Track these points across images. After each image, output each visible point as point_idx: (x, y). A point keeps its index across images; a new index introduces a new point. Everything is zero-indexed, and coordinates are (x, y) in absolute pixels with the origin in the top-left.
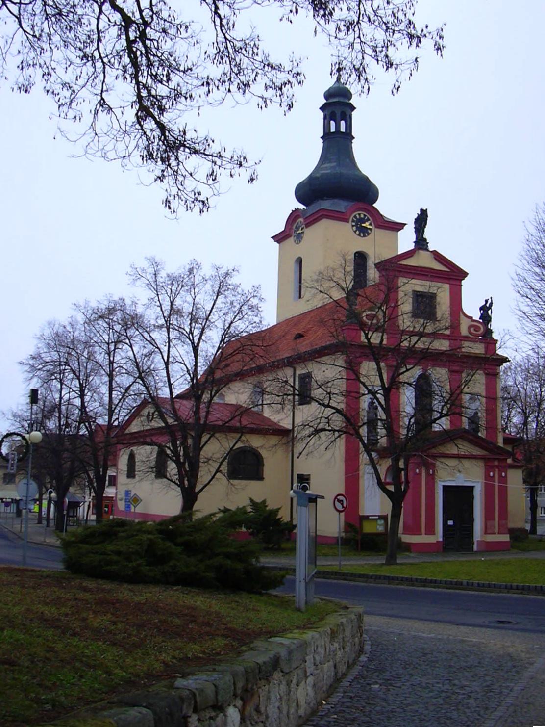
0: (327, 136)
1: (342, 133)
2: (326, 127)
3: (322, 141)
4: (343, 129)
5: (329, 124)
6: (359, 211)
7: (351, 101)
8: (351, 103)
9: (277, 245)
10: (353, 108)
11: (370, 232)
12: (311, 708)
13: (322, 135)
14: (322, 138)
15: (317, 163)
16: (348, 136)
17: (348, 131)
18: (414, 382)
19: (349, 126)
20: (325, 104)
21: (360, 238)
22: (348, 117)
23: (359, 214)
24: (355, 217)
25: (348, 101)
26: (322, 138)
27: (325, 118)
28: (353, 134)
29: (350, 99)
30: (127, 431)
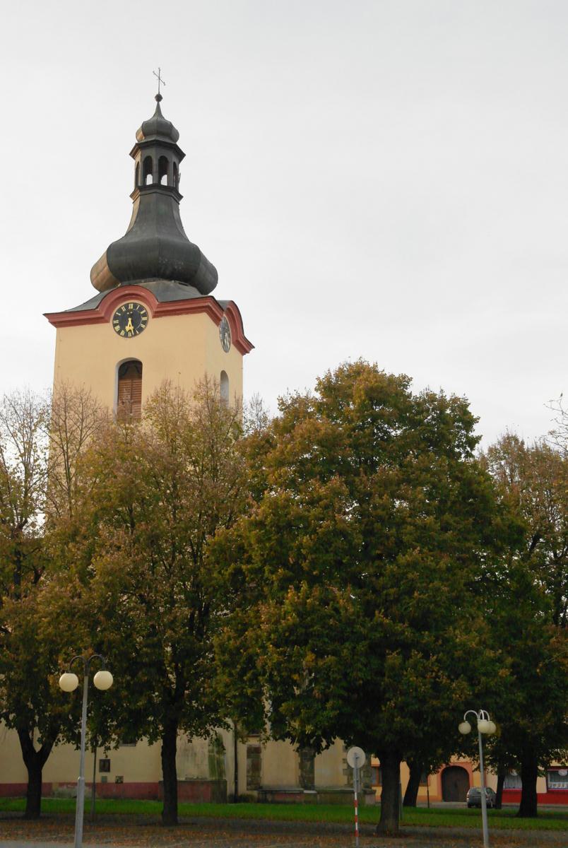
9: (53, 329)
11: (143, 326)
16: (173, 194)
24: (120, 310)
28: (181, 191)
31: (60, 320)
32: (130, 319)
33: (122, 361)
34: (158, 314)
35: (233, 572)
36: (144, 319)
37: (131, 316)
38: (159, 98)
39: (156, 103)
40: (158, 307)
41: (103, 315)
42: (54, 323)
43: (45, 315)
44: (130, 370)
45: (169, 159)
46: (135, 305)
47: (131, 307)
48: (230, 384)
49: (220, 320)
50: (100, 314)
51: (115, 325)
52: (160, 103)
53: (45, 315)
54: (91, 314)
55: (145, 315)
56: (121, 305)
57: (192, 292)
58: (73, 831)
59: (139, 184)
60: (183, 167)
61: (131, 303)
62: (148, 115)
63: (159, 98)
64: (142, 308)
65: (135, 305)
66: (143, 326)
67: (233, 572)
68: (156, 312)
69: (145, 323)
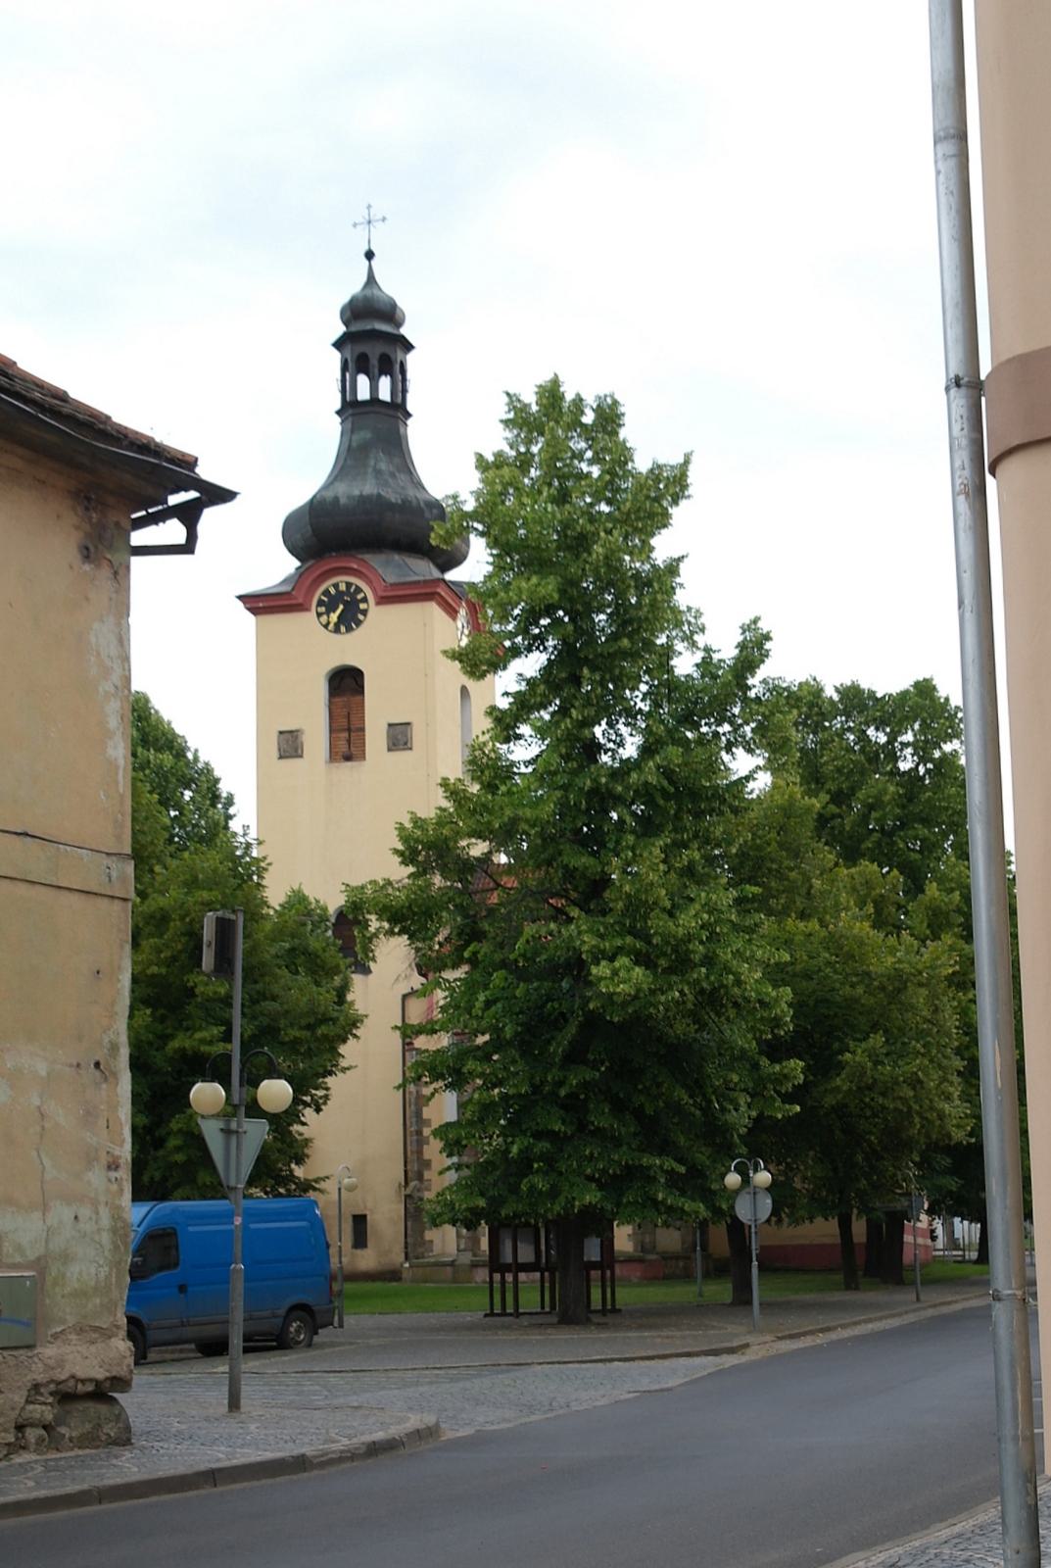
0: (350, 408)
1: (384, 403)
2: (347, 388)
3: (338, 420)
4: (385, 394)
5: (393, 393)
6: (318, 586)
7: (403, 331)
8: (403, 337)
9: (250, 618)
10: (408, 347)
11: (361, 617)
12: (953, 137)
13: (338, 406)
14: (338, 413)
15: (331, 467)
16: (397, 409)
17: (399, 400)
18: (527, 763)
19: (400, 388)
20: (345, 334)
21: (327, 632)
22: (397, 367)
23: (336, 586)
24: (326, 593)
25: (395, 332)
26: (338, 413)
27: (344, 368)
28: (410, 407)
29: (399, 325)
30: (621, 554)
31: (259, 604)
32: (341, 607)
33: (333, 669)
34: (383, 600)
35: (190, 1053)
36: (362, 606)
37: (346, 603)
38: (370, 255)
39: (367, 262)
40: (385, 591)
41: (300, 601)
42: (255, 611)
43: (240, 597)
44: (346, 683)
45: (392, 356)
46: (349, 585)
47: (343, 587)
48: (473, 709)
49: (456, 612)
50: (295, 598)
51: (319, 615)
52: (372, 262)
53: (240, 597)
54: (399, 590)
55: (365, 600)
56: (328, 584)
57: (424, 569)
58: (763, 1248)
59: (348, 399)
60: (412, 360)
61: (342, 580)
62: (354, 286)
63: (370, 255)
64: (359, 590)
65: (349, 585)
66: (361, 617)
67: (190, 1053)
68: (382, 597)
69: (365, 612)
